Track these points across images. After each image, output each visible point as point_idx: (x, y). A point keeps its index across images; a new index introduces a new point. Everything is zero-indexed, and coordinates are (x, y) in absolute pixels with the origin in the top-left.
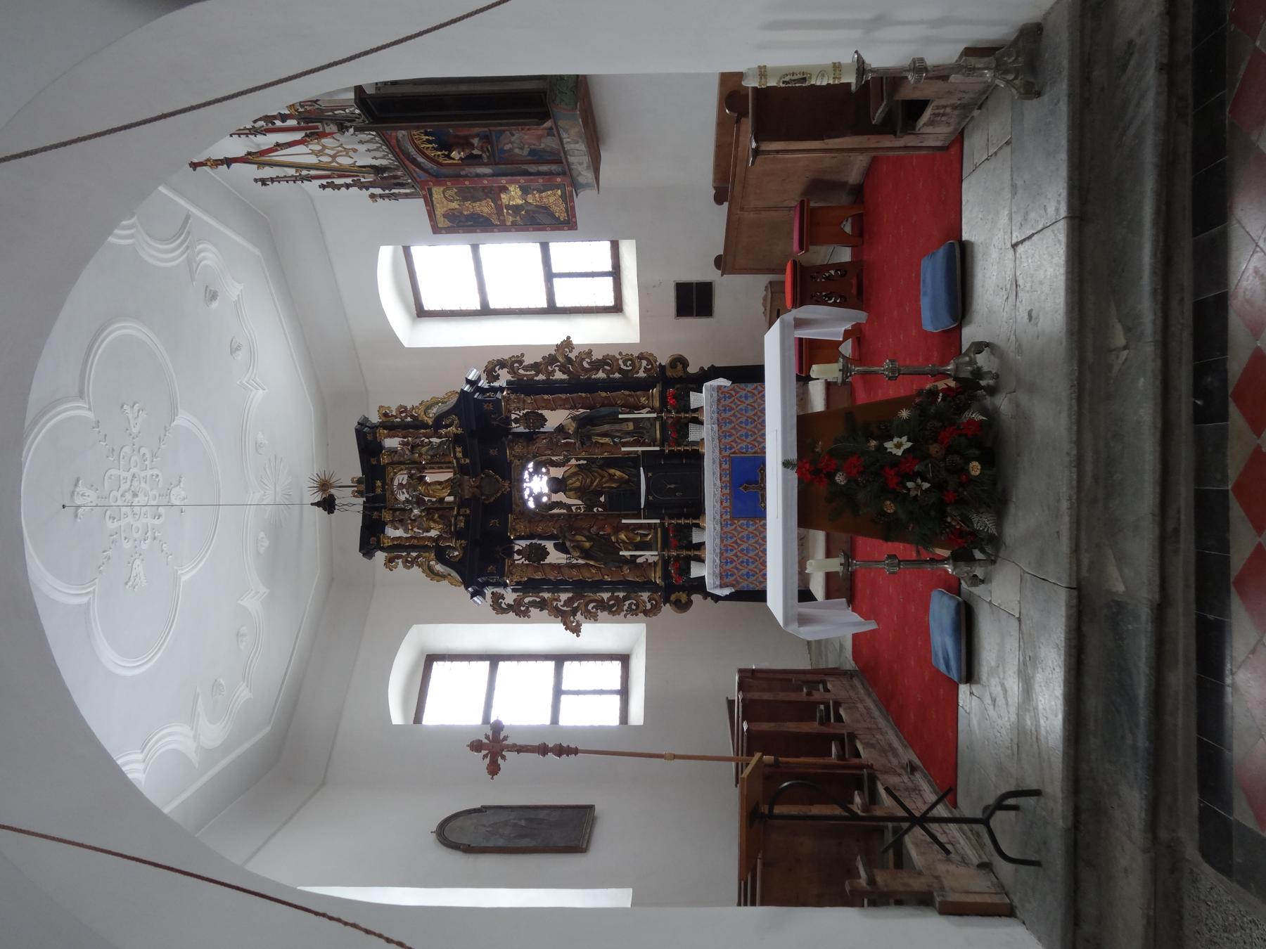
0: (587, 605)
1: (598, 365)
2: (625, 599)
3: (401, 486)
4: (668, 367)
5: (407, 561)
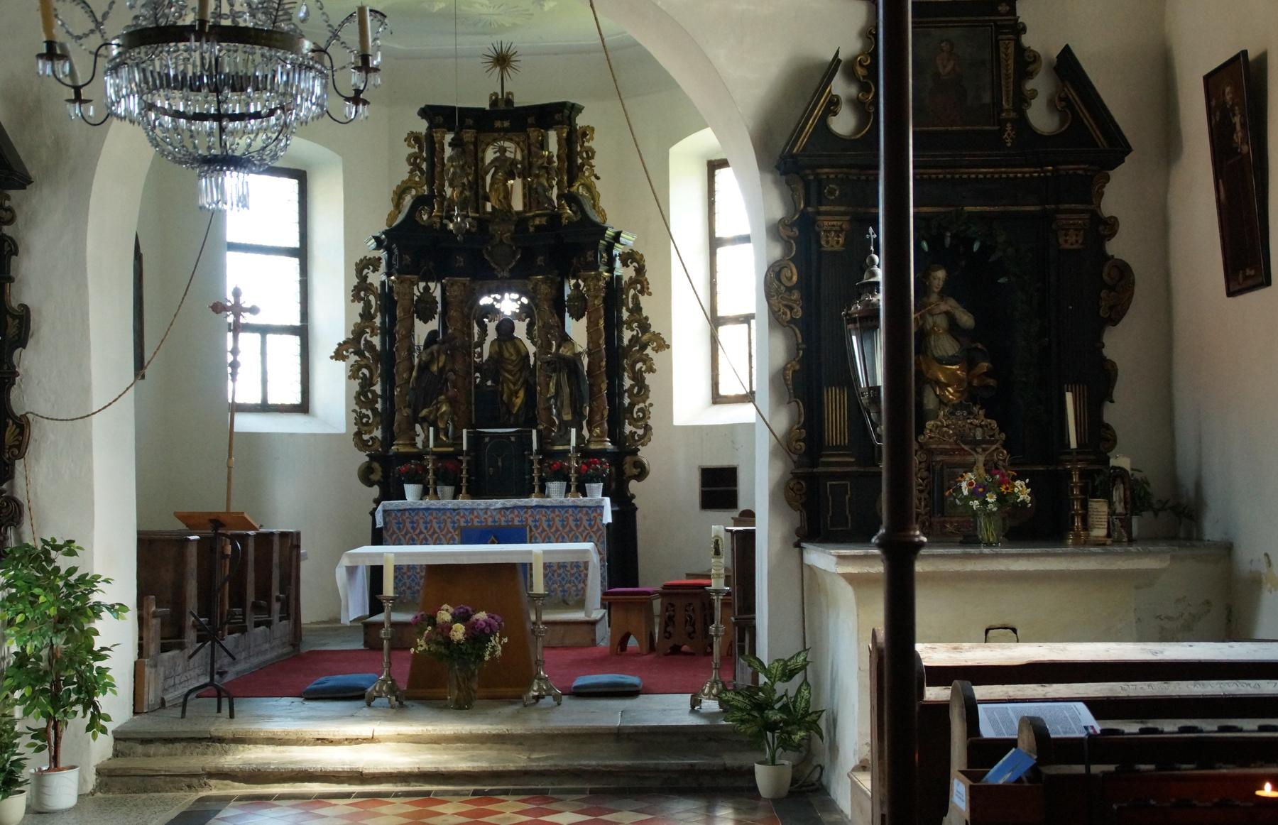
0: (367, 367)
1: (638, 379)
2: (374, 410)
3: (503, 150)
4: (635, 458)
5: (416, 159)
